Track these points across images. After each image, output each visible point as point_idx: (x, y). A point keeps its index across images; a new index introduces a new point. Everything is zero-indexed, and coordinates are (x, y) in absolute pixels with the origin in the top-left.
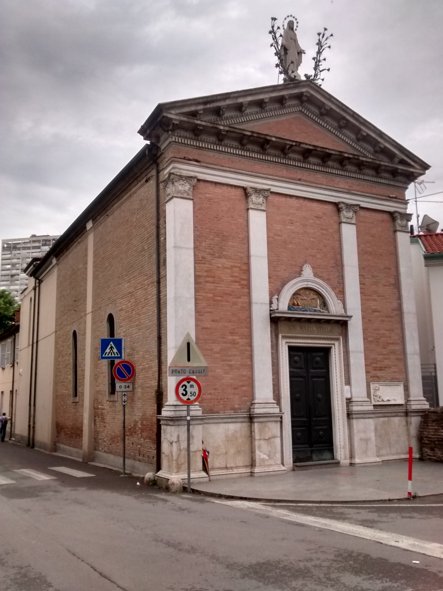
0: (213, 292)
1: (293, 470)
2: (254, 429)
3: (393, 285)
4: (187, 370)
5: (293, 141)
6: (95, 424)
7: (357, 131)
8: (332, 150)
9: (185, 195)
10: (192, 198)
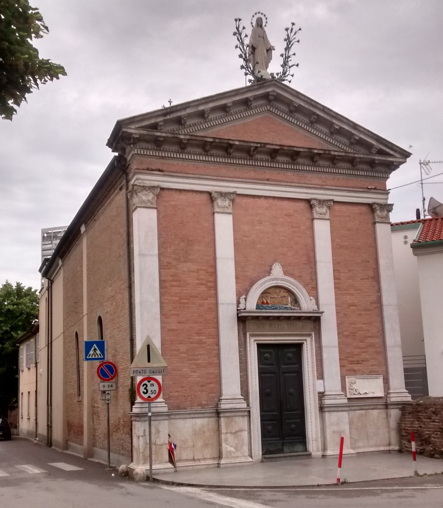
0: (178, 295)
1: (262, 462)
2: (221, 424)
3: (372, 278)
4: (148, 370)
5: (257, 143)
6: (93, 422)
7: (330, 125)
8: (300, 147)
9: (149, 205)
10: (155, 206)
